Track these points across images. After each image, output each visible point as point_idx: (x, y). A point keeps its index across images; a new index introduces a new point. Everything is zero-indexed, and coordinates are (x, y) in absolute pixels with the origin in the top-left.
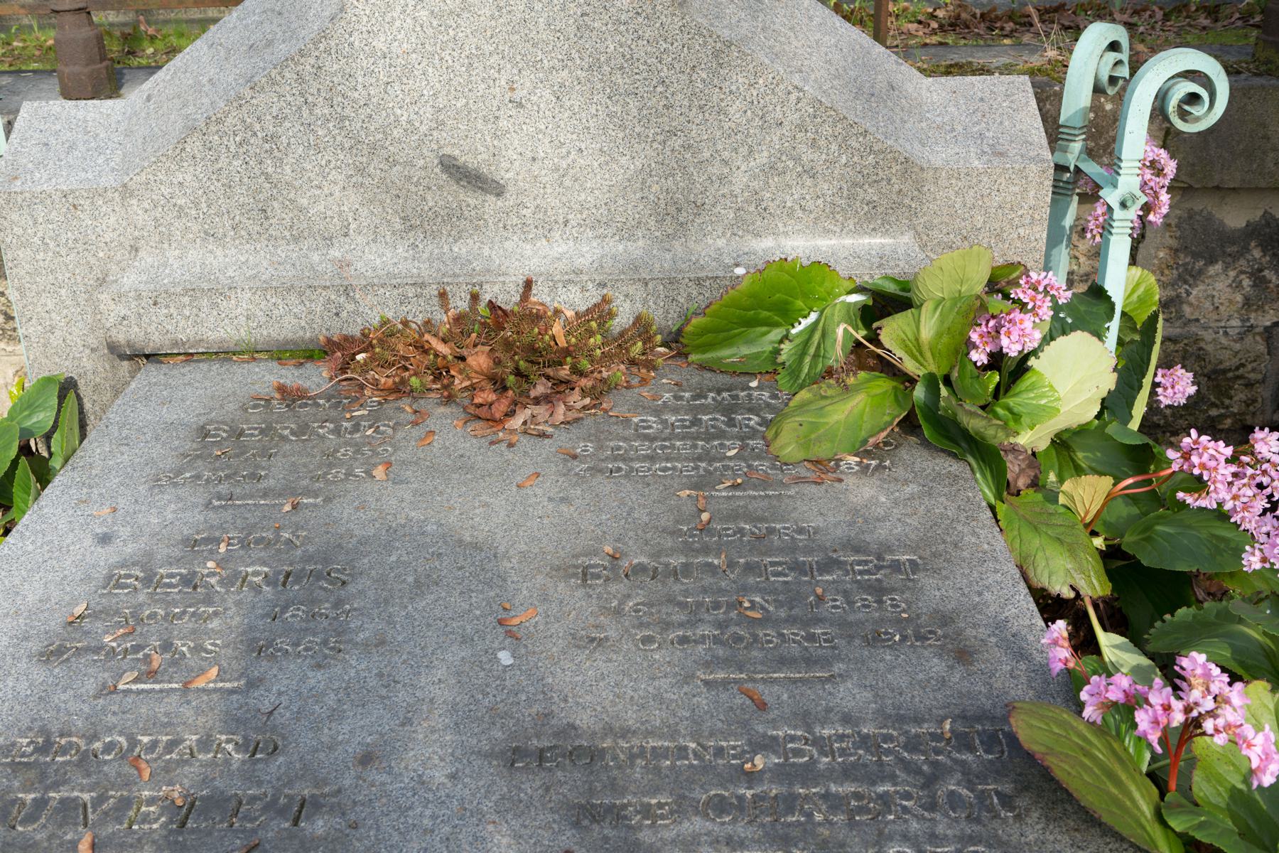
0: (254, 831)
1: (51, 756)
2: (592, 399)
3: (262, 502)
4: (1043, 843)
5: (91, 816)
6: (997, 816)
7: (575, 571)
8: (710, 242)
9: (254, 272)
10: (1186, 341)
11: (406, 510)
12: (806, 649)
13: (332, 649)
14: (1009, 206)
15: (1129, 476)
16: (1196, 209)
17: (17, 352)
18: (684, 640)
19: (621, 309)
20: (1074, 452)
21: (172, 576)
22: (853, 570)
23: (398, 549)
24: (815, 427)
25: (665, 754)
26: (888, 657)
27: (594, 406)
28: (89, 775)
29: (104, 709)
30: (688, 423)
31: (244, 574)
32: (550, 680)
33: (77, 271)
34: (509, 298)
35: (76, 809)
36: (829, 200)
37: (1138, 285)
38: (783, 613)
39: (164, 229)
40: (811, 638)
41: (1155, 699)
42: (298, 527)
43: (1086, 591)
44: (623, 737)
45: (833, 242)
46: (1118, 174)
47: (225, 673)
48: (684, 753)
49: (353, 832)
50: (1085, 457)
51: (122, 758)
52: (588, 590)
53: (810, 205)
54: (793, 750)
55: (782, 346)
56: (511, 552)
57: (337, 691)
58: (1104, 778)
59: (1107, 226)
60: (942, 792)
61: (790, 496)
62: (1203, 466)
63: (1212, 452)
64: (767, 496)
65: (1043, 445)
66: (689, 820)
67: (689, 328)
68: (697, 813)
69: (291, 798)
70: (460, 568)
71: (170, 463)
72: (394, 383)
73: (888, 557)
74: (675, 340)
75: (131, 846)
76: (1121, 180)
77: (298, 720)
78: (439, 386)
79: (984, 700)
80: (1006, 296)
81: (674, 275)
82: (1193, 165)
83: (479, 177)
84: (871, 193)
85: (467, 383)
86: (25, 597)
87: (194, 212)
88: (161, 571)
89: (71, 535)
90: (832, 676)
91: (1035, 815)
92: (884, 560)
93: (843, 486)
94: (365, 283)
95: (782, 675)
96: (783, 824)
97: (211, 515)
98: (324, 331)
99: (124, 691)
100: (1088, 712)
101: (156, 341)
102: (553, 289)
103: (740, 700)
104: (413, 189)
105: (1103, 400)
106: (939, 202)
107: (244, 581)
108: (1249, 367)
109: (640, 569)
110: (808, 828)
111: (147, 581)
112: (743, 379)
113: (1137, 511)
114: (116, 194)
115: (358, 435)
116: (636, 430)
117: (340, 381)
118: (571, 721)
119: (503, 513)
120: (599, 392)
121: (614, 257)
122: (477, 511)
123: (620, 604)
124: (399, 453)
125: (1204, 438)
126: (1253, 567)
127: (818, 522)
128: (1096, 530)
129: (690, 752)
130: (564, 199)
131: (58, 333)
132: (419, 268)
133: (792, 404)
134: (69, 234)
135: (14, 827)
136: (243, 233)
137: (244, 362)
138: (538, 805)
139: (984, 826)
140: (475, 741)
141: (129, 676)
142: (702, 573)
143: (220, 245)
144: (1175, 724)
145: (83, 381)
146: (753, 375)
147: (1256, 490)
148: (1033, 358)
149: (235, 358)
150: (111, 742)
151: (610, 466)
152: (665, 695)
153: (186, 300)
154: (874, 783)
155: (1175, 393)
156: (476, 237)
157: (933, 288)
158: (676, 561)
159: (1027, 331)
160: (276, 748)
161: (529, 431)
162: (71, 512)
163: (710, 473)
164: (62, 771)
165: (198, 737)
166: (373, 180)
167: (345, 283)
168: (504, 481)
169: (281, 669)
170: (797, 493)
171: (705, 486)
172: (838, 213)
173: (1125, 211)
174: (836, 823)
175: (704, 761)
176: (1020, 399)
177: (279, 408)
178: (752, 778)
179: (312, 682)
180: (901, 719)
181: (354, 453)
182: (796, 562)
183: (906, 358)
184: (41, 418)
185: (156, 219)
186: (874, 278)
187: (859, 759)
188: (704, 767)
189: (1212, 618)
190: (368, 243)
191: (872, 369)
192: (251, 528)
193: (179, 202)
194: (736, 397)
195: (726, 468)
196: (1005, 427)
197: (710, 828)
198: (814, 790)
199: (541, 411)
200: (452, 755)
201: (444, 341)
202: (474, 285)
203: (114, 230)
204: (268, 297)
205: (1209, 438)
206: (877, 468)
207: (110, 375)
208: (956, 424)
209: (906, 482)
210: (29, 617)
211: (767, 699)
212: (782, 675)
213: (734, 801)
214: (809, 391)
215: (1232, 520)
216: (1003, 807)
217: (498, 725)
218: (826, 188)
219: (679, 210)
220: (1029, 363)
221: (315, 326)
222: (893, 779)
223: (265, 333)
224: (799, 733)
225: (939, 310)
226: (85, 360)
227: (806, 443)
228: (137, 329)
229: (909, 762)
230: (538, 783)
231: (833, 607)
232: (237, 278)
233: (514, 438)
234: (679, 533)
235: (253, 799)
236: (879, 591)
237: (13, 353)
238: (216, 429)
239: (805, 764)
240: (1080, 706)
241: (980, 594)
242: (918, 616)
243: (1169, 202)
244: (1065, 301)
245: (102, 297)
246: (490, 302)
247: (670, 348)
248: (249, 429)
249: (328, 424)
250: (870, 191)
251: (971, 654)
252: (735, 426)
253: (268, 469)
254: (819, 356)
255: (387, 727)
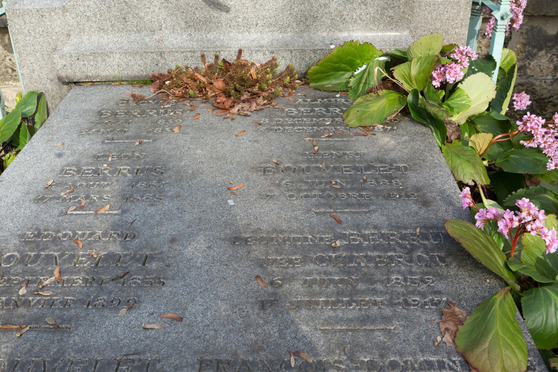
0: (126, 267)
1: (41, 238)
2: (268, 101)
3: (126, 141)
4: (457, 275)
5: (58, 261)
6: (438, 265)
7: (260, 169)
8: (320, 34)
9: (121, 46)
10: (527, 85)
11: (188, 145)
12: (359, 200)
13: (157, 198)
14: (451, 19)
15: (499, 134)
16: (535, 25)
17: (17, 86)
18: (306, 196)
19: (280, 63)
20: (476, 125)
21: (89, 170)
22: (379, 170)
23: (185, 160)
24: (364, 112)
25: (299, 239)
26: (394, 204)
27: (269, 104)
28: (57, 246)
29: (62, 221)
30: (309, 111)
31: (119, 169)
32: (250, 211)
33: (44, 45)
34: (232, 58)
35: (52, 258)
36: (372, 15)
37: (507, 56)
38: (349, 186)
39: (81, 27)
40: (361, 196)
41: (507, 216)
42: (142, 151)
43: (479, 183)
44: (281, 233)
45: (374, 34)
46: (501, 4)
47: (112, 207)
48: (306, 240)
49: (168, 268)
50: (481, 127)
51: (70, 239)
52: (266, 176)
53: (364, 18)
54: (352, 239)
55: (351, 79)
56: (233, 161)
57: (160, 215)
58: (483, 249)
59: (494, 28)
60: (414, 256)
61: (353, 141)
62: (532, 128)
63: (536, 121)
64: (343, 140)
65: (463, 122)
66: (308, 265)
67: (310, 71)
68: (312, 262)
69: (141, 255)
70: (211, 168)
71: (86, 125)
72: (182, 93)
73: (395, 165)
74: (305, 78)
75: (76, 272)
76: (502, 7)
77: (144, 225)
78: (201, 96)
79: (434, 221)
80: (449, 58)
81: (304, 48)
82: (534, 5)
83: (219, 4)
84: (391, 13)
85: (213, 94)
86: (27, 178)
87: (94, 19)
88: (84, 168)
89: (45, 154)
90: (369, 211)
91: (454, 265)
92: (393, 166)
93: (376, 137)
94: (169, 51)
95: (348, 210)
96: (348, 267)
97: (105, 146)
98: (151, 72)
99: (70, 214)
100: (478, 224)
101: (78, 76)
102: (251, 54)
103: (330, 219)
104: (190, 9)
105: (490, 103)
106: (421, 17)
107: (119, 172)
108: (555, 97)
109: (289, 168)
110: (358, 269)
111: (78, 172)
112: (333, 94)
113: (503, 150)
114: (60, 11)
115: (167, 115)
116: (287, 114)
117: (158, 93)
118: (259, 227)
119: (229, 146)
120: (271, 98)
121: (278, 40)
122: (218, 145)
123: (279, 182)
124: (184, 122)
125: (533, 116)
126: (551, 168)
127: (365, 151)
128: (485, 158)
129: (309, 239)
130: (256, 14)
131: (36, 73)
132: (192, 45)
133: (354, 104)
134: (40, 28)
135: (27, 265)
136: (116, 28)
137: (117, 85)
138: (245, 258)
139: (432, 268)
140: (218, 234)
141: (72, 208)
142: (315, 170)
143: (106, 34)
144: (514, 226)
145: (47, 94)
146: (337, 92)
147: (554, 139)
148: (460, 84)
149: (113, 84)
150: (65, 233)
151: (275, 128)
152: (298, 217)
153: (91, 58)
154: (386, 252)
155: (521, 104)
156: (217, 31)
157: (418, 53)
158: (304, 166)
159: (458, 72)
160: (135, 236)
161: (241, 114)
162: (45, 145)
163: (319, 131)
164: (46, 244)
165: (102, 232)
166: (172, 5)
167: (161, 51)
168: (230, 133)
169: (136, 206)
170: (356, 139)
171: (316, 136)
172: (376, 21)
173: (503, 21)
174: (370, 267)
175: (315, 242)
176: (452, 102)
177: (132, 104)
178: (335, 249)
179: (150, 211)
180: (398, 228)
181: (165, 122)
182: (355, 166)
183: (405, 83)
184: (30, 108)
185: (78, 22)
186: (392, 50)
187: (380, 243)
188: (315, 245)
189: (533, 193)
190: (170, 34)
191: (389, 89)
192: (123, 151)
193: (88, 14)
194: (330, 101)
195: (325, 129)
196: (446, 111)
197: (317, 268)
198: (361, 254)
199: (246, 106)
200: (209, 239)
201: (204, 76)
202: (216, 52)
203: (60, 27)
204: (127, 57)
205: (535, 116)
206: (390, 130)
207: (59, 91)
208: (425, 110)
209: (403, 135)
210: (29, 185)
211: (342, 219)
212: (348, 210)
213: (327, 258)
214: (362, 98)
215: (544, 152)
216: (441, 262)
217: (228, 228)
218: (371, 10)
219: (306, 19)
220: (458, 86)
221: (147, 70)
222: (394, 250)
223: (126, 73)
224: (355, 232)
225: (419, 62)
226: (48, 85)
227: (360, 119)
228: (70, 71)
229: (401, 244)
230: (245, 250)
231: (371, 184)
232: (113, 48)
233: (234, 117)
234: (305, 155)
235: (125, 256)
236: (390, 178)
237: (15, 86)
238: (105, 112)
239: (358, 244)
240: (474, 222)
241: (433, 180)
242: (407, 188)
243: (522, 19)
244: (475, 59)
245: (54, 56)
246: (224, 59)
247: (302, 81)
248: (120, 112)
249: (154, 110)
250: (390, 11)
251: (429, 203)
252: (330, 113)
253: (129, 128)
254: (367, 83)
255: (181, 229)
